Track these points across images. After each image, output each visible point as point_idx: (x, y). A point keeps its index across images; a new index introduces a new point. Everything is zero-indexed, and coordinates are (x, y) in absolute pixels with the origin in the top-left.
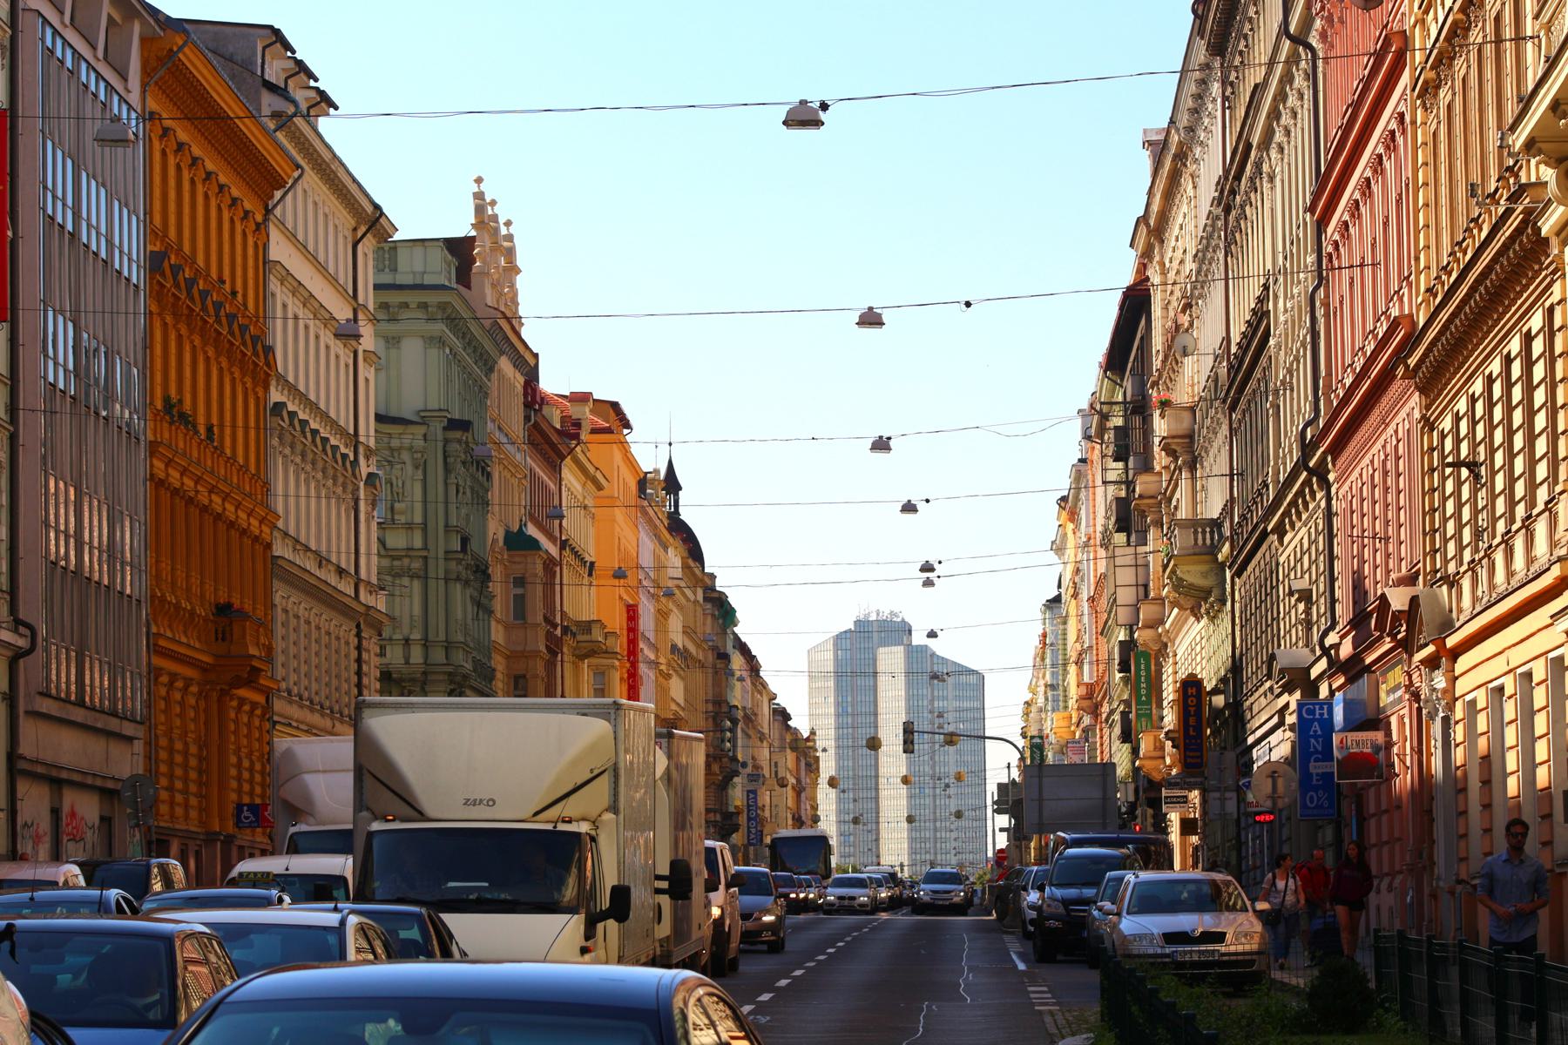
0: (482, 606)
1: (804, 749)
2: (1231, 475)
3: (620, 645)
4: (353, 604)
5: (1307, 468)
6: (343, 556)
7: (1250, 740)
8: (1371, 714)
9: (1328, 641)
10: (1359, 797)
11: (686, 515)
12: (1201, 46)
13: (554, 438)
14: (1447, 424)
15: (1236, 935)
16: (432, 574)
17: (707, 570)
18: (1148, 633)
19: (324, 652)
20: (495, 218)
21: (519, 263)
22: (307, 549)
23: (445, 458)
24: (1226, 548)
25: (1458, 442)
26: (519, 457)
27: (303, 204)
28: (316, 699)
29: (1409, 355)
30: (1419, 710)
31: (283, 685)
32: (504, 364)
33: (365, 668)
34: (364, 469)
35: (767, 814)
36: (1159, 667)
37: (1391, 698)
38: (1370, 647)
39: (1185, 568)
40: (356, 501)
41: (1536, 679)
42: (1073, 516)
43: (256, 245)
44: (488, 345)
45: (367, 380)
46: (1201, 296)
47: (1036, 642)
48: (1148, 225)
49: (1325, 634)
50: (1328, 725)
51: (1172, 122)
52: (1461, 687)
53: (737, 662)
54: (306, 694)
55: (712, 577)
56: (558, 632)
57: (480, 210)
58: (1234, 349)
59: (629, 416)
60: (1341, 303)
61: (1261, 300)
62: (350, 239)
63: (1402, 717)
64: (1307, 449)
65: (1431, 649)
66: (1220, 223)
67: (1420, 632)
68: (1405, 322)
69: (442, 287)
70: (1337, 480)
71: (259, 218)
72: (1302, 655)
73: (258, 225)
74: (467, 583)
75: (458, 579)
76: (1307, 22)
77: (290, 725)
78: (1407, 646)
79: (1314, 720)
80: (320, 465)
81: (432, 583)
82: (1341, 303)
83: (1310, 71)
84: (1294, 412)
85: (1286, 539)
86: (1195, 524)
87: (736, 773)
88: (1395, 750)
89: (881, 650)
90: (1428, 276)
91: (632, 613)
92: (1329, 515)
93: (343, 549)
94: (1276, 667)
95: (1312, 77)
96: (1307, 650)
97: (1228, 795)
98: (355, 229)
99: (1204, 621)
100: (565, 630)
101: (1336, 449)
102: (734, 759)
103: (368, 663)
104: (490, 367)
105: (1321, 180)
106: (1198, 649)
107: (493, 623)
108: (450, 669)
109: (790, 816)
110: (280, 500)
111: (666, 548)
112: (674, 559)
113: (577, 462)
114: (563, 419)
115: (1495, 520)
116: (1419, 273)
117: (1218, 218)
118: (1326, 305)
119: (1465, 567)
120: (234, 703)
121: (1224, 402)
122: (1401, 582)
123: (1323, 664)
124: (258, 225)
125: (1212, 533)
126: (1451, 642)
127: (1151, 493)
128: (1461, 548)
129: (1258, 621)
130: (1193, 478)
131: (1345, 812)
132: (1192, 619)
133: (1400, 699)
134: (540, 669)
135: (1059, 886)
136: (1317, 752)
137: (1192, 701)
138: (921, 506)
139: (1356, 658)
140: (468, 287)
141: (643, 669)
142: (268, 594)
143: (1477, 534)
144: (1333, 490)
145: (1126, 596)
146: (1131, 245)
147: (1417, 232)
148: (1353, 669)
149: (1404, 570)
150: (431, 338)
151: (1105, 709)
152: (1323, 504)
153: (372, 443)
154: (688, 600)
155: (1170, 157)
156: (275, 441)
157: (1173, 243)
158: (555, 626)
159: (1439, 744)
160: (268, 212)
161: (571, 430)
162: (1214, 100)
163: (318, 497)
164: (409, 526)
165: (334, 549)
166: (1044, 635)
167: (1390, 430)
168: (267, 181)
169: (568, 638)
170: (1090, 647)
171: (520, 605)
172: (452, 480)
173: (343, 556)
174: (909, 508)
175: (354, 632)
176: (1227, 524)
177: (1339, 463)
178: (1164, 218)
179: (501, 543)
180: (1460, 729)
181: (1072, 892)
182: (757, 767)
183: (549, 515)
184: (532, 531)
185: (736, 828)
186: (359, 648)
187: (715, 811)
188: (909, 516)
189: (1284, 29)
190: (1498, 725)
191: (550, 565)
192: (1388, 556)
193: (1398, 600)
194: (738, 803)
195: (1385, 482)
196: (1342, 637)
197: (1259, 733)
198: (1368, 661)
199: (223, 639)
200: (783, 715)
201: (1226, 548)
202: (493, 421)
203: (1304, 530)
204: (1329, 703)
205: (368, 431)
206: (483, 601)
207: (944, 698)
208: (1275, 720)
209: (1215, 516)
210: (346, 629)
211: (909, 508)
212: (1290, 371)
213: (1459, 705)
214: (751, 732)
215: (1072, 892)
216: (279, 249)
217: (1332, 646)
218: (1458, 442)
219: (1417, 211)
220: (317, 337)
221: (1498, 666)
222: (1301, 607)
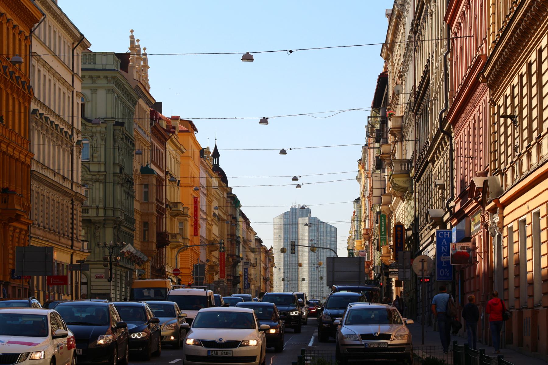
0: (130, 195)
1: (268, 253)
2: (415, 140)
3: (190, 212)
4: (70, 192)
5: (443, 131)
6: (66, 172)
7: (421, 248)
8: (467, 236)
10: (462, 272)
11: (221, 166)
13: (163, 132)
14: (501, 102)
15: (396, 336)
16: (108, 181)
17: (229, 186)
18: (385, 207)
19: (56, 210)
20: (139, 46)
22: (48, 168)
23: (114, 136)
25: (506, 108)
26: (147, 138)
27: (46, 29)
28: (52, 228)
29: (484, 71)
30: (488, 232)
31: (36, 222)
32: (141, 102)
33: (75, 217)
34: (76, 139)
35: (252, 277)
37: (476, 228)
38: (467, 205)
39: (397, 179)
40: (72, 151)
41: (541, 215)
42: (363, 167)
43: (26, 46)
44: (133, 94)
45: (78, 103)
48: (387, 47)
49: (449, 201)
52: (506, 221)
53: (240, 219)
54: (47, 226)
55: (231, 189)
56: (164, 206)
57: (132, 42)
58: (417, 90)
59: (196, 126)
61: (427, 67)
62: (71, 47)
63: (480, 236)
64: (442, 122)
65: (493, 203)
68: (483, 57)
69: (114, 70)
71: (27, 34)
72: (441, 211)
73: (26, 38)
74: (122, 186)
75: (118, 183)
77: (38, 238)
78: (482, 204)
80: (55, 135)
81: (108, 184)
84: (438, 106)
86: (402, 162)
87: (239, 262)
88: (477, 251)
89: (300, 219)
90: (493, 36)
91: (196, 201)
92: (452, 150)
93: (66, 168)
97: (407, 270)
98: (73, 44)
99: (405, 202)
100: (167, 206)
101: (454, 122)
102: (238, 256)
103: (76, 215)
104: (135, 103)
106: (403, 213)
107: (134, 201)
108: (114, 219)
109: (262, 278)
110: (36, 146)
111: (211, 177)
112: (215, 182)
113: (172, 141)
114: (167, 126)
115: (522, 141)
116: (490, 35)
117: (411, 37)
118: (451, 61)
119: (509, 165)
120: (12, 229)
123: (448, 216)
124: (26, 38)
125: (408, 165)
126: (502, 200)
127: (387, 152)
128: (507, 157)
129: (425, 202)
133: (480, 228)
135: (329, 308)
136: (444, 252)
137: (399, 233)
139: (461, 211)
140: (127, 72)
141: (201, 221)
142: (29, 185)
143: (514, 149)
144: (453, 140)
145: (377, 193)
146: (381, 55)
147: (489, 17)
148: (460, 216)
149: (482, 170)
150: (109, 90)
151: (373, 238)
152: (449, 147)
153: (80, 128)
154: (220, 197)
156: (34, 125)
157: (396, 53)
158: (163, 204)
159: (496, 247)
160: (31, 32)
163: (49, 145)
164: (99, 163)
165: (61, 168)
166: (354, 212)
167: (477, 109)
168: (31, 20)
171: (146, 194)
172: (117, 145)
173: (66, 172)
174: (283, 152)
175: (70, 202)
176: (414, 162)
177: (455, 128)
178: (393, 43)
179: (139, 171)
180: (505, 240)
181: (335, 311)
182: (248, 260)
184: (153, 167)
185: (239, 282)
186: (72, 209)
187: (231, 276)
190: (523, 248)
191: (160, 181)
192: (475, 165)
193: (479, 182)
194: (241, 273)
195: (474, 132)
198: (466, 212)
199: (5, 202)
200: (259, 241)
202: (136, 124)
203: (442, 159)
205: (78, 124)
206: (131, 193)
208: (430, 240)
209: (409, 158)
210: (67, 201)
211: (283, 152)
212: (437, 93)
213: (505, 229)
215: (335, 311)
216: (36, 47)
218: (506, 108)
219: (489, 7)
220: (55, 85)
221: (524, 209)
222: (440, 191)
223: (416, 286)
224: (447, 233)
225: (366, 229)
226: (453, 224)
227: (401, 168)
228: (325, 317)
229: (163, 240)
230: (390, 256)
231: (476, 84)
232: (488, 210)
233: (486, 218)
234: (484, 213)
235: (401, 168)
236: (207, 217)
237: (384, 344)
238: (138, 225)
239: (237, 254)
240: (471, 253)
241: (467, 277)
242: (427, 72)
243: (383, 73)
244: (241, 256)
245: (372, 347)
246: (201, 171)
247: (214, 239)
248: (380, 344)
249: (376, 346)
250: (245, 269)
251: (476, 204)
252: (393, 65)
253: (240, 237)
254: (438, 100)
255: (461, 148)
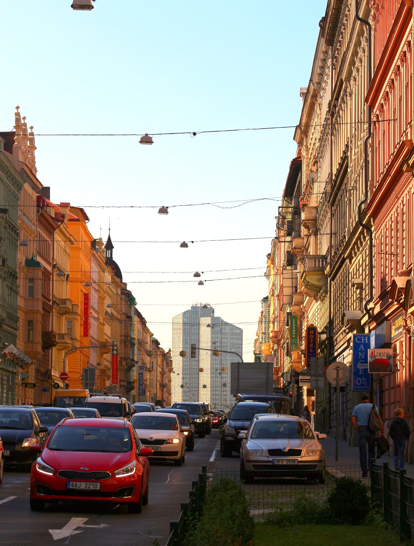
1: (166, 357)
2: (331, 234)
3: (80, 310)
5: (362, 225)
7: (336, 354)
8: (387, 341)
9: (369, 307)
10: (381, 381)
11: (115, 258)
12: (323, 40)
13: (50, 220)
18: (296, 308)
20: (25, 124)
21: (36, 145)
24: (328, 268)
26: (33, 227)
30: (410, 338)
32: (27, 186)
36: (301, 323)
37: (397, 333)
38: (387, 308)
42: (273, 262)
46: (321, 157)
47: (260, 314)
48: (301, 129)
49: (368, 302)
50: (368, 346)
51: (311, 80)
53: (136, 319)
55: (125, 284)
56: (51, 303)
57: (18, 120)
58: (334, 178)
60: (379, 144)
61: (345, 153)
64: (362, 214)
66: (329, 122)
67: (411, 298)
70: (375, 230)
72: (358, 313)
76: (367, 12)
79: (361, 343)
82: (379, 144)
83: (368, 38)
85: (353, 261)
86: (316, 257)
87: (134, 366)
91: (86, 297)
94: (346, 319)
95: (369, 41)
96: (360, 312)
97: (320, 378)
99: (319, 302)
100: (54, 302)
101: (375, 215)
102: (133, 360)
104: (20, 188)
105: (371, 82)
106: (316, 314)
107: (18, 297)
109: (158, 384)
112: (108, 277)
114: (56, 214)
117: (328, 119)
118: (372, 146)
121: (329, 202)
122: (403, 274)
123: (366, 318)
125: (322, 261)
129: (341, 301)
130: (316, 238)
131: (374, 388)
132: (314, 301)
133: (401, 333)
134: (40, 318)
137: (312, 337)
138: (190, 244)
139: (381, 313)
140: (11, 153)
141: (91, 321)
144: (373, 235)
145: (287, 291)
146: (294, 139)
148: (379, 319)
149: (404, 269)
151: (282, 342)
155: (310, 97)
158: (49, 301)
161: (60, 218)
162: (329, 67)
166: (262, 312)
167: (400, 201)
169: (55, 306)
170: (277, 316)
174: (184, 245)
176: (329, 258)
177: (376, 222)
178: (308, 126)
179: (23, 263)
182: (144, 363)
183: (45, 250)
184: (39, 259)
185: (133, 388)
187: (124, 381)
188: (184, 249)
189: (357, 17)
191: (47, 275)
192: (397, 263)
193: (401, 282)
194: (135, 378)
196: (375, 305)
197: (339, 351)
198: (386, 315)
200: (156, 343)
201: (328, 268)
203: (360, 255)
204: (368, 336)
206: (14, 288)
207: (226, 338)
208: (346, 345)
209: (324, 254)
212: (356, 182)
214: (142, 349)
215: (239, 423)
217: (370, 309)
222: (358, 291)
223: (330, 396)
224: (365, 338)
225: (275, 332)
226: (371, 328)
227: (315, 264)
228: (228, 430)
229: (49, 341)
230: (301, 362)
231: (399, 173)
232: (411, 313)
233: (408, 321)
234: (406, 316)
235: (315, 264)
236: (98, 316)
237: (294, 461)
238: (21, 324)
239: (131, 358)
240: (391, 361)
241: (387, 387)
242: (345, 158)
243: (296, 158)
244: (136, 359)
245: (280, 463)
246: (93, 265)
247: (106, 340)
248: (289, 460)
249: (285, 463)
250: (139, 373)
251: (397, 306)
252: (307, 150)
253: (134, 338)
254: (356, 190)
255: (382, 244)
